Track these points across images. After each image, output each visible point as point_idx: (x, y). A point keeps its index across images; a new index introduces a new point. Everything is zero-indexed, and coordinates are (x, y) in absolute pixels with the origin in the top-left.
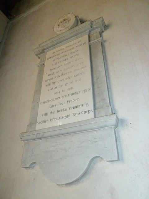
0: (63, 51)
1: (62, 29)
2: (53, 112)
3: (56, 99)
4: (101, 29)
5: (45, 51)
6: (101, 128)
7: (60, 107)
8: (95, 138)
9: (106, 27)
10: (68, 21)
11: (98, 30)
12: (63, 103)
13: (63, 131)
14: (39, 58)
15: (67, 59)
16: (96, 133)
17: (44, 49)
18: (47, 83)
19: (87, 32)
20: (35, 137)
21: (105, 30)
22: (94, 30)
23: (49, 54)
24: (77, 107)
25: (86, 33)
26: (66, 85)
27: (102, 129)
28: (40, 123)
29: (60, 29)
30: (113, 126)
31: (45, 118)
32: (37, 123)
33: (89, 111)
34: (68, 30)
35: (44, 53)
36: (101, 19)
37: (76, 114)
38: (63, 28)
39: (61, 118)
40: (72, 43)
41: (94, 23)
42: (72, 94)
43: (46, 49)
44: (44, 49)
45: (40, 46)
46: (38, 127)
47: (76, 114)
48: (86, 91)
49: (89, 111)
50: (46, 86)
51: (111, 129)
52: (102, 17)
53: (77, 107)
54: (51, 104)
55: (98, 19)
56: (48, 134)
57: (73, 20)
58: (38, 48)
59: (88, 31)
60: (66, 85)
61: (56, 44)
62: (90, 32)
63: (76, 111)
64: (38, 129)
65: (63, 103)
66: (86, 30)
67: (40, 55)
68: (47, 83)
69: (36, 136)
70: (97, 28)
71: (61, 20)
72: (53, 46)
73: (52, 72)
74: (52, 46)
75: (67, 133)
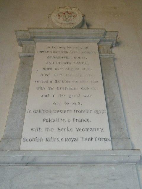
0: (61, 50)
1: (64, 22)
2: (50, 128)
3: (55, 111)
4: (112, 44)
5: (34, 39)
6: (121, 163)
7: (62, 125)
8: (113, 175)
9: (118, 44)
10: (73, 17)
11: (110, 43)
12: (66, 120)
13: (69, 160)
14: (21, 45)
15: (70, 63)
16: (114, 169)
17: (34, 37)
18: (40, 85)
19: (97, 40)
20: (19, 160)
21: (116, 46)
22: (105, 41)
23: (40, 46)
24: (88, 130)
25: (96, 41)
26: (70, 96)
27: (123, 165)
28: (28, 140)
29: (61, 21)
30: (84, 28)
31: (37, 135)
32: (22, 140)
33: (106, 140)
34: (73, 28)
35: (32, 41)
36: (116, 34)
37: (86, 140)
38: (66, 22)
39: (64, 139)
40: (66, 45)
41: (108, 34)
42: (80, 112)
43: (36, 38)
44: (34, 37)
45: (30, 30)
46: (24, 146)
47: (86, 140)
48: (99, 112)
49: (106, 140)
50: (38, 89)
51: (132, 166)
52: (118, 32)
53: (88, 130)
54: (47, 116)
55: (113, 32)
56: (45, 160)
57: (78, 20)
58: (25, 31)
59: (99, 40)
60: (70, 96)
61: (54, 38)
62: (100, 41)
63: (88, 135)
64: (24, 149)
65: (66, 120)
66: (96, 38)
67: (25, 42)
68: (40, 85)
69: (22, 159)
70: (109, 41)
71: (62, 10)
72: (50, 39)
73: (46, 72)
74: (46, 38)
75: (74, 163)
